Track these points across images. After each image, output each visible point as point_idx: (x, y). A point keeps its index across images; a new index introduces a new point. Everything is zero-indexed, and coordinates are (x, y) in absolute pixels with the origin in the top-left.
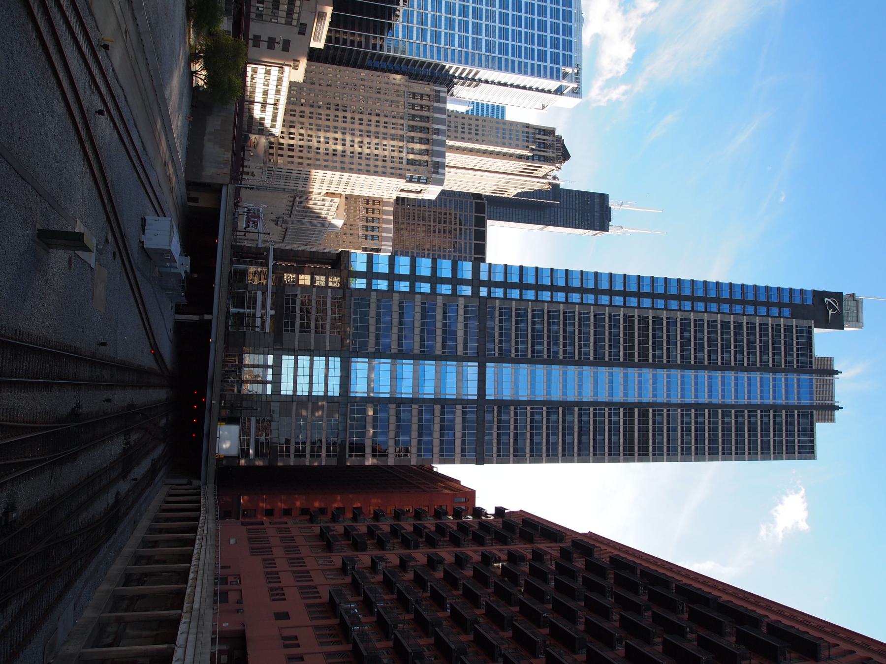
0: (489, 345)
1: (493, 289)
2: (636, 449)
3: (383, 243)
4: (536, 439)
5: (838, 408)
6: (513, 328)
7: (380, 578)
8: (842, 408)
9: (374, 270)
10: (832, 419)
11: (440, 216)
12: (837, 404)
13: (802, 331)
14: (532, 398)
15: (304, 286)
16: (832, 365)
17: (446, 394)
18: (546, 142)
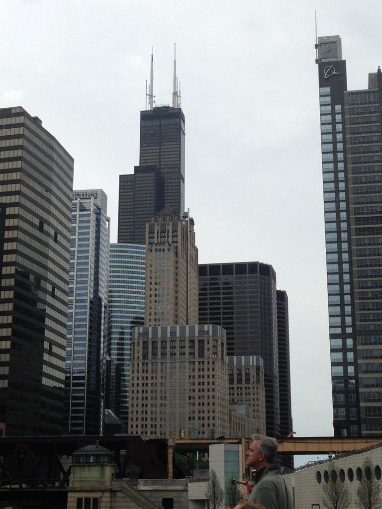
1: (347, 324)
3: (251, 364)
6: (373, 312)
8: (379, 67)
13: (353, 100)
15: (10, 371)
16: (374, 74)
18: (160, 232)
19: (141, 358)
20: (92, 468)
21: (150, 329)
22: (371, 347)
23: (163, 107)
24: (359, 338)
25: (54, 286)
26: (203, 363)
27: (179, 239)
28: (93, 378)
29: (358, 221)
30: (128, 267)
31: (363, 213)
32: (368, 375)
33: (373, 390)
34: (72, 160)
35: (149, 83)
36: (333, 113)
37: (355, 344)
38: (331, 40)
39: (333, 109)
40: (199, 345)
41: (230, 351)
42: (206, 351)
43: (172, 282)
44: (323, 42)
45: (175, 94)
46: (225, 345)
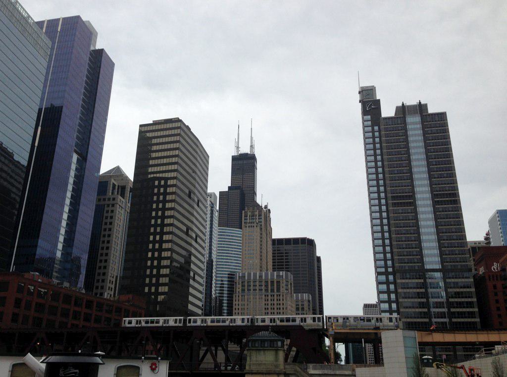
0: (417, 268)
2: (453, 199)
3: (305, 299)
4: (457, 252)
9: (387, 300)
10: (426, 105)
11: (261, 288)
13: (387, 122)
16: (400, 107)
20: (266, 352)
21: (246, 274)
22: (407, 281)
24: (398, 275)
25: (197, 236)
26: (280, 295)
27: (263, 220)
30: (226, 241)
31: (397, 193)
32: (406, 300)
33: (410, 310)
34: (208, 157)
35: (237, 140)
36: (373, 132)
38: (369, 88)
39: (373, 129)
40: (273, 287)
42: (281, 288)
43: (259, 245)
45: (252, 147)
46: (293, 285)
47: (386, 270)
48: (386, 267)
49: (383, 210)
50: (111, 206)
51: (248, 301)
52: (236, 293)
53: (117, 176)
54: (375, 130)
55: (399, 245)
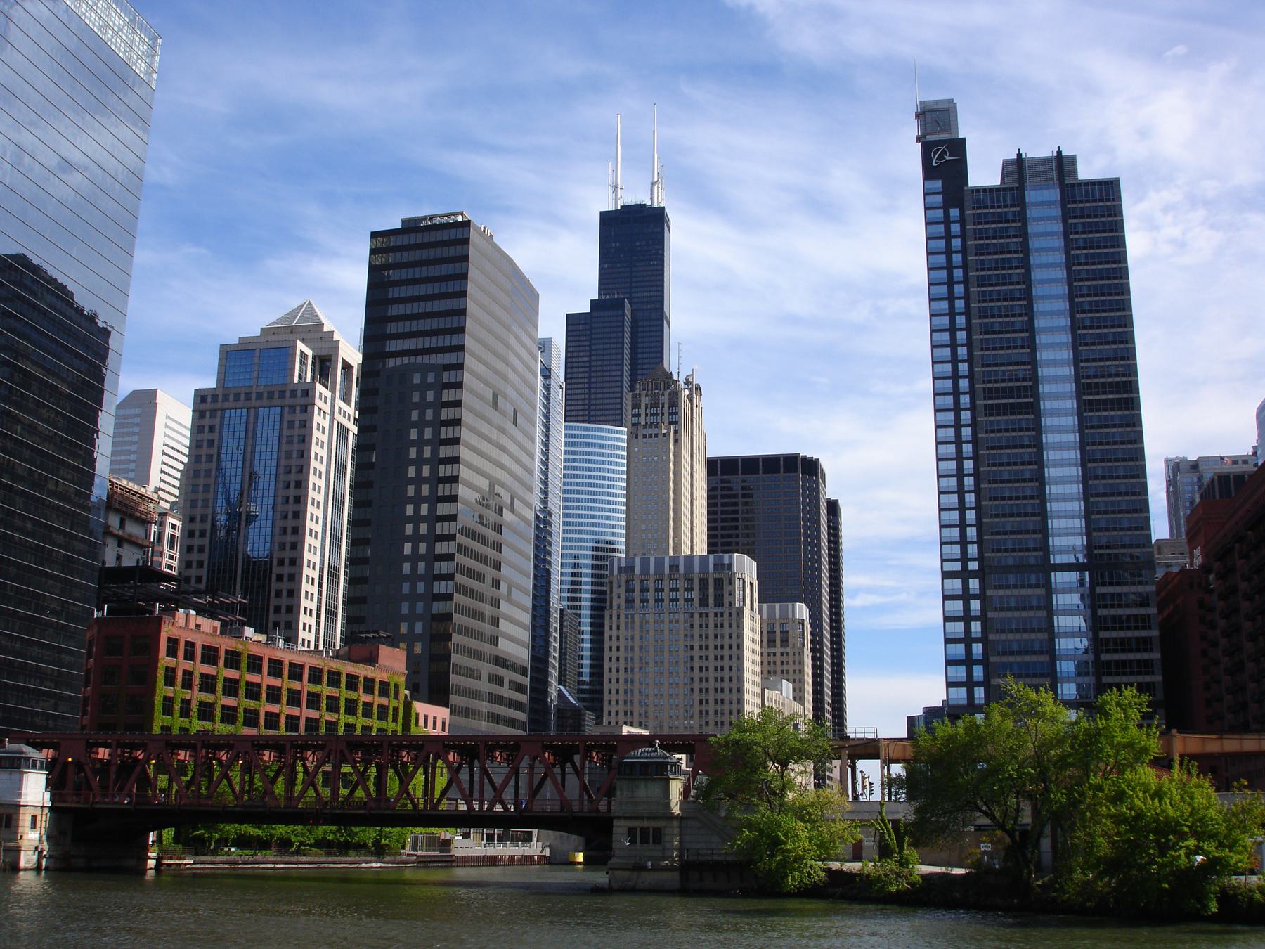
0: (1032, 561)
1: (965, 472)
2: (1125, 396)
5: (1059, 152)
7: (1255, 576)
8: (1059, 147)
9: (964, 680)
10: (1072, 159)
12: (1055, 155)
13: (978, 201)
14: (1063, 265)
16: (1012, 161)
17: (1080, 510)
19: (623, 605)
23: (636, 205)
28: (541, 636)
29: (989, 393)
31: (996, 381)
36: (947, 221)
37: (983, 587)
39: (947, 215)
41: (602, 596)
44: (927, 108)
47: (965, 566)
48: (964, 559)
49: (968, 522)
50: (298, 409)
51: (641, 627)
52: (611, 608)
53: (309, 329)
54: (953, 249)
55: (982, 262)
